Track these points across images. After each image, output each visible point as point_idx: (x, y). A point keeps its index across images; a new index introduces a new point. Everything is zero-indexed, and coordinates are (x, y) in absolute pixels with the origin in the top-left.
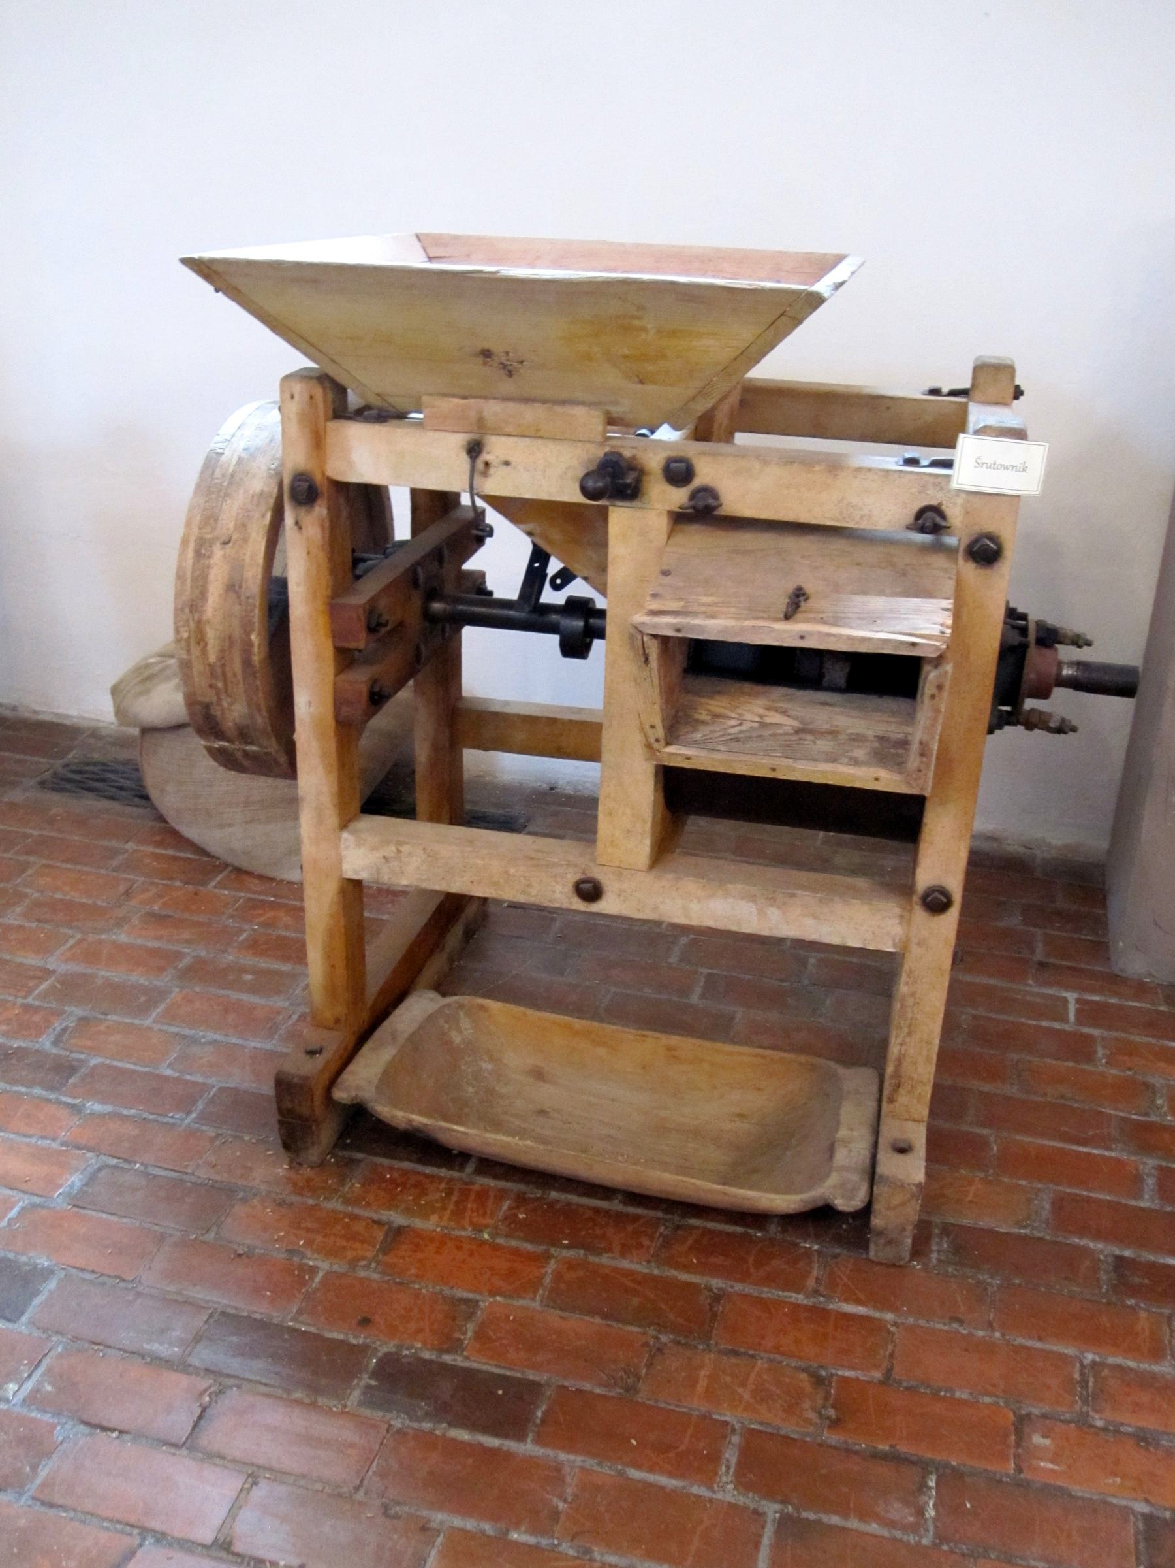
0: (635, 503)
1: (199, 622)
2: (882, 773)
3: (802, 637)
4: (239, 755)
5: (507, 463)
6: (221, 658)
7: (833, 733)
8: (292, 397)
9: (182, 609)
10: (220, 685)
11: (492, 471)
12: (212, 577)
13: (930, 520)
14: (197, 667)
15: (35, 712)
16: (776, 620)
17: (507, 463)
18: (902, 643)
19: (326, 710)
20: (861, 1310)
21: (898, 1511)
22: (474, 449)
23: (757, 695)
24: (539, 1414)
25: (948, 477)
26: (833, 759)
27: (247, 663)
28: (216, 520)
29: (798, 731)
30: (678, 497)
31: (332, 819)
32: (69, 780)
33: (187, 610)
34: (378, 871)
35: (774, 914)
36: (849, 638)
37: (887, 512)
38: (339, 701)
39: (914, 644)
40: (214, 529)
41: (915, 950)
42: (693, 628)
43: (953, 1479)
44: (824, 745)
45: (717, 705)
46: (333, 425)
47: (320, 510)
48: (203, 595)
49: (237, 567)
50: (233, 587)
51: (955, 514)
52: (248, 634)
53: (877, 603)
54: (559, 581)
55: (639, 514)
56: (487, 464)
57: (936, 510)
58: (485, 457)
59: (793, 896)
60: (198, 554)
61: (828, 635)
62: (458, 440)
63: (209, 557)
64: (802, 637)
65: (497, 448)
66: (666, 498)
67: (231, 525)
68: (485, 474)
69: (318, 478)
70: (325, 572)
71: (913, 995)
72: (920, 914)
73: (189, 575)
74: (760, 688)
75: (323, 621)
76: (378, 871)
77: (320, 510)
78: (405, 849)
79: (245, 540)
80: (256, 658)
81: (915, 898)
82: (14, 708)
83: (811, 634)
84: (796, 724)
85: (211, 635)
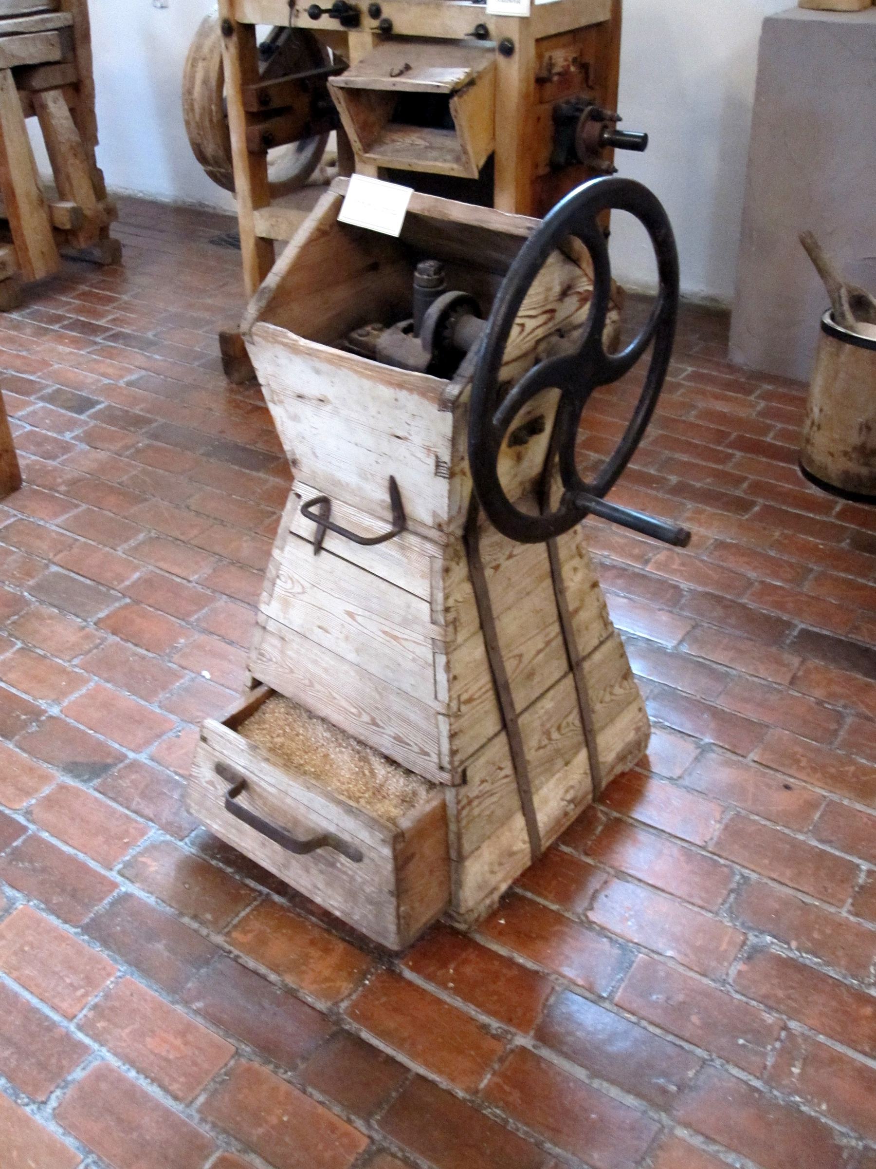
0: (357, 29)
2: (455, 166)
3: (394, 85)
4: (218, 175)
6: (201, 118)
7: (441, 149)
10: (202, 133)
11: (300, 15)
14: (193, 124)
15: (225, 211)
16: (383, 75)
19: (243, 145)
23: (414, 132)
25: (484, 8)
26: (436, 160)
27: (211, 121)
29: (426, 147)
30: (375, 23)
31: (249, 204)
32: (225, 241)
34: (270, 232)
36: (412, 84)
37: (461, 28)
38: (249, 140)
39: (438, 86)
42: (352, 82)
44: (435, 154)
45: (395, 136)
47: (235, 38)
49: (207, 72)
50: (205, 82)
51: (492, 27)
52: (210, 105)
53: (438, 70)
55: (359, 34)
57: (482, 26)
61: (404, 83)
64: (394, 85)
66: (369, 24)
68: (297, 16)
69: (233, 23)
70: (238, 72)
74: (419, 129)
75: (239, 97)
76: (270, 232)
77: (235, 38)
78: (280, 220)
80: (215, 119)
82: (214, 208)
84: (427, 144)
85: (197, 107)
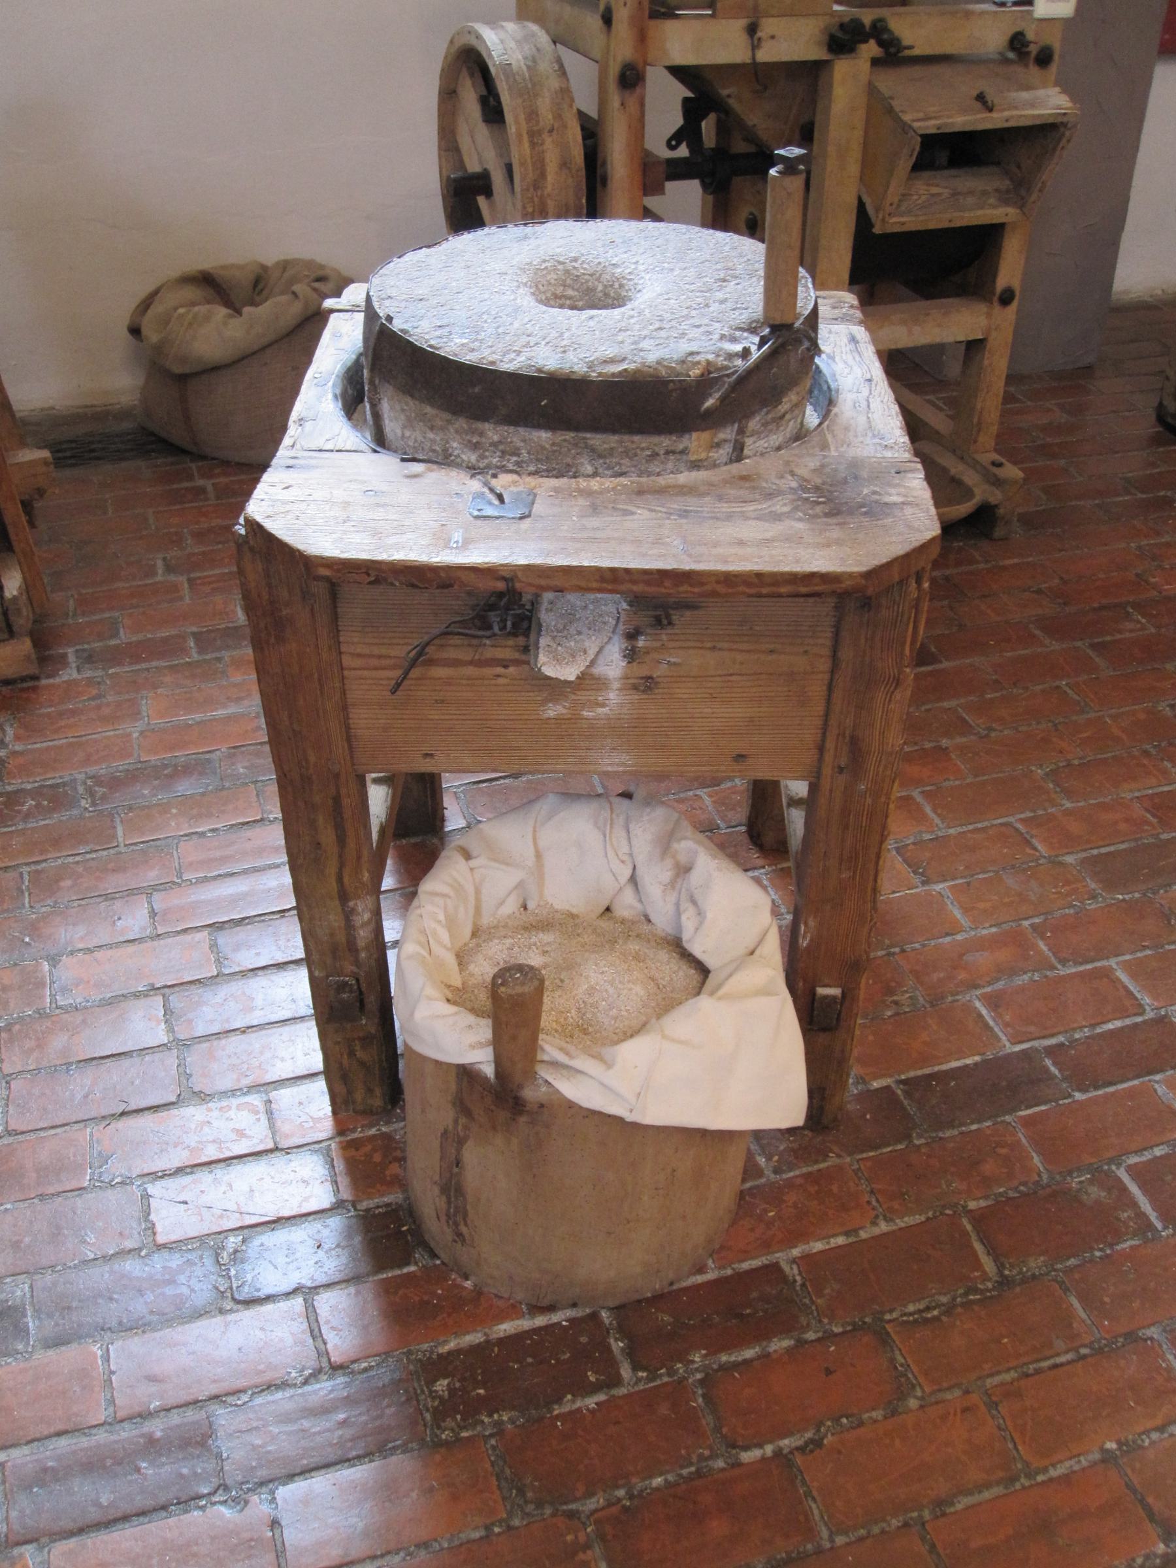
0: (853, 55)
1: (541, 197)
5: (773, 37)
7: (971, 193)
8: (625, 4)
9: (528, 190)
12: (547, 160)
13: (1017, 42)
17: (773, 37)
18: (1059, 114)
20: (1016, 561)
21: (1129, 625)
22: (752, 29)
24: (933, 650)
28: (537, 115)
33: (532, 189)
35: (917, 329)
36: (1033, 116)
39: (1065, 114)
40: (538, 123)
41: (994, 334)
42: (946, 125)
43: (1137, 606)
44: (970, 200)
46: (652, 23)
48: (543, 175)
50: (564, 164)
54: (674, 143)
56: (759, 39)
58: (759, 34)
59: (928, 314)
60: (533, 145)
61: (1021, 116)
62: (742, 23)
63: (542, 144)
65: (769, 26)
67: (550, 117)
71: (990, 365)
72: (997, 308)
73: (529, 160)
79: (565, 127)
81: (996, 298)
83: (1012, 117)
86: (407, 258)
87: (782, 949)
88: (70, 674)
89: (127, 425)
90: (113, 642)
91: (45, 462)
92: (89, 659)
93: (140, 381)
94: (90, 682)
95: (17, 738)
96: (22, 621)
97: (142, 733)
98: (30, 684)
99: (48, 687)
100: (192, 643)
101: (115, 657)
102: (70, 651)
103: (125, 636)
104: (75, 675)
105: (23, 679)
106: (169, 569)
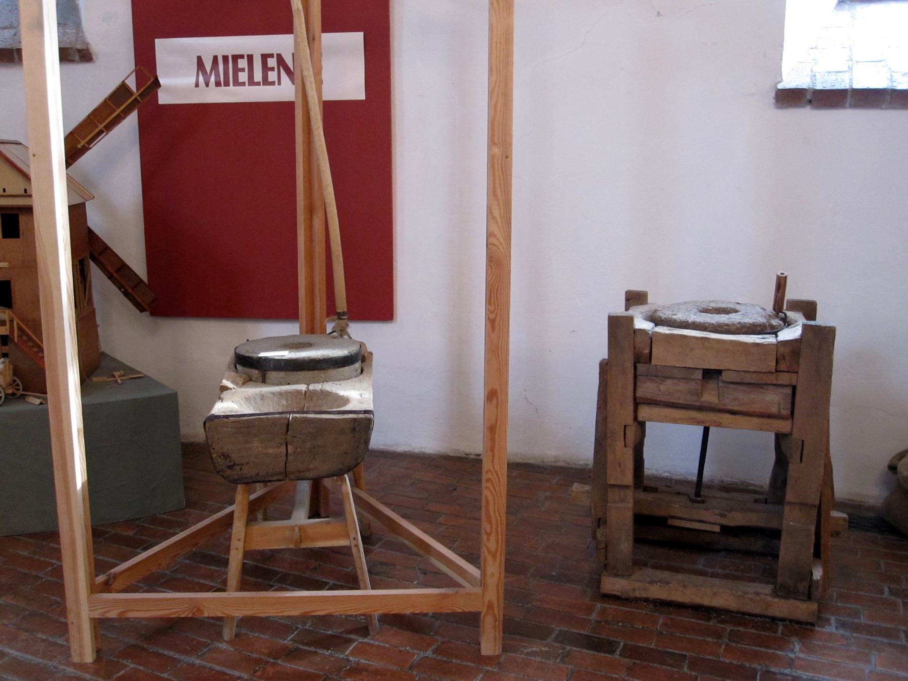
86: (98, 322)
87: (787, 107)
88: (831, 629)
89: (871, 514)
90: (856, 621)
91: (844, 519)
92: (842, 625)
93: (885, 494)
94: (842, 636)
95: (801, 651)
96: (817, 593)
97: (870, 672)
98: (808, 627)
99: (818, 631)
100: (903, 635)
101: (857, 628)
102: (833, 619)
103: (863, 620)
104: (834, 630)
105: (807, 623)
106: (891, 592)
